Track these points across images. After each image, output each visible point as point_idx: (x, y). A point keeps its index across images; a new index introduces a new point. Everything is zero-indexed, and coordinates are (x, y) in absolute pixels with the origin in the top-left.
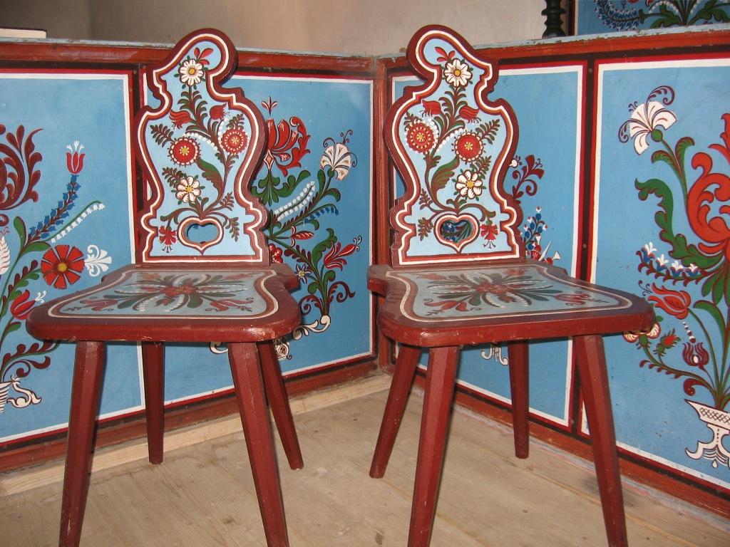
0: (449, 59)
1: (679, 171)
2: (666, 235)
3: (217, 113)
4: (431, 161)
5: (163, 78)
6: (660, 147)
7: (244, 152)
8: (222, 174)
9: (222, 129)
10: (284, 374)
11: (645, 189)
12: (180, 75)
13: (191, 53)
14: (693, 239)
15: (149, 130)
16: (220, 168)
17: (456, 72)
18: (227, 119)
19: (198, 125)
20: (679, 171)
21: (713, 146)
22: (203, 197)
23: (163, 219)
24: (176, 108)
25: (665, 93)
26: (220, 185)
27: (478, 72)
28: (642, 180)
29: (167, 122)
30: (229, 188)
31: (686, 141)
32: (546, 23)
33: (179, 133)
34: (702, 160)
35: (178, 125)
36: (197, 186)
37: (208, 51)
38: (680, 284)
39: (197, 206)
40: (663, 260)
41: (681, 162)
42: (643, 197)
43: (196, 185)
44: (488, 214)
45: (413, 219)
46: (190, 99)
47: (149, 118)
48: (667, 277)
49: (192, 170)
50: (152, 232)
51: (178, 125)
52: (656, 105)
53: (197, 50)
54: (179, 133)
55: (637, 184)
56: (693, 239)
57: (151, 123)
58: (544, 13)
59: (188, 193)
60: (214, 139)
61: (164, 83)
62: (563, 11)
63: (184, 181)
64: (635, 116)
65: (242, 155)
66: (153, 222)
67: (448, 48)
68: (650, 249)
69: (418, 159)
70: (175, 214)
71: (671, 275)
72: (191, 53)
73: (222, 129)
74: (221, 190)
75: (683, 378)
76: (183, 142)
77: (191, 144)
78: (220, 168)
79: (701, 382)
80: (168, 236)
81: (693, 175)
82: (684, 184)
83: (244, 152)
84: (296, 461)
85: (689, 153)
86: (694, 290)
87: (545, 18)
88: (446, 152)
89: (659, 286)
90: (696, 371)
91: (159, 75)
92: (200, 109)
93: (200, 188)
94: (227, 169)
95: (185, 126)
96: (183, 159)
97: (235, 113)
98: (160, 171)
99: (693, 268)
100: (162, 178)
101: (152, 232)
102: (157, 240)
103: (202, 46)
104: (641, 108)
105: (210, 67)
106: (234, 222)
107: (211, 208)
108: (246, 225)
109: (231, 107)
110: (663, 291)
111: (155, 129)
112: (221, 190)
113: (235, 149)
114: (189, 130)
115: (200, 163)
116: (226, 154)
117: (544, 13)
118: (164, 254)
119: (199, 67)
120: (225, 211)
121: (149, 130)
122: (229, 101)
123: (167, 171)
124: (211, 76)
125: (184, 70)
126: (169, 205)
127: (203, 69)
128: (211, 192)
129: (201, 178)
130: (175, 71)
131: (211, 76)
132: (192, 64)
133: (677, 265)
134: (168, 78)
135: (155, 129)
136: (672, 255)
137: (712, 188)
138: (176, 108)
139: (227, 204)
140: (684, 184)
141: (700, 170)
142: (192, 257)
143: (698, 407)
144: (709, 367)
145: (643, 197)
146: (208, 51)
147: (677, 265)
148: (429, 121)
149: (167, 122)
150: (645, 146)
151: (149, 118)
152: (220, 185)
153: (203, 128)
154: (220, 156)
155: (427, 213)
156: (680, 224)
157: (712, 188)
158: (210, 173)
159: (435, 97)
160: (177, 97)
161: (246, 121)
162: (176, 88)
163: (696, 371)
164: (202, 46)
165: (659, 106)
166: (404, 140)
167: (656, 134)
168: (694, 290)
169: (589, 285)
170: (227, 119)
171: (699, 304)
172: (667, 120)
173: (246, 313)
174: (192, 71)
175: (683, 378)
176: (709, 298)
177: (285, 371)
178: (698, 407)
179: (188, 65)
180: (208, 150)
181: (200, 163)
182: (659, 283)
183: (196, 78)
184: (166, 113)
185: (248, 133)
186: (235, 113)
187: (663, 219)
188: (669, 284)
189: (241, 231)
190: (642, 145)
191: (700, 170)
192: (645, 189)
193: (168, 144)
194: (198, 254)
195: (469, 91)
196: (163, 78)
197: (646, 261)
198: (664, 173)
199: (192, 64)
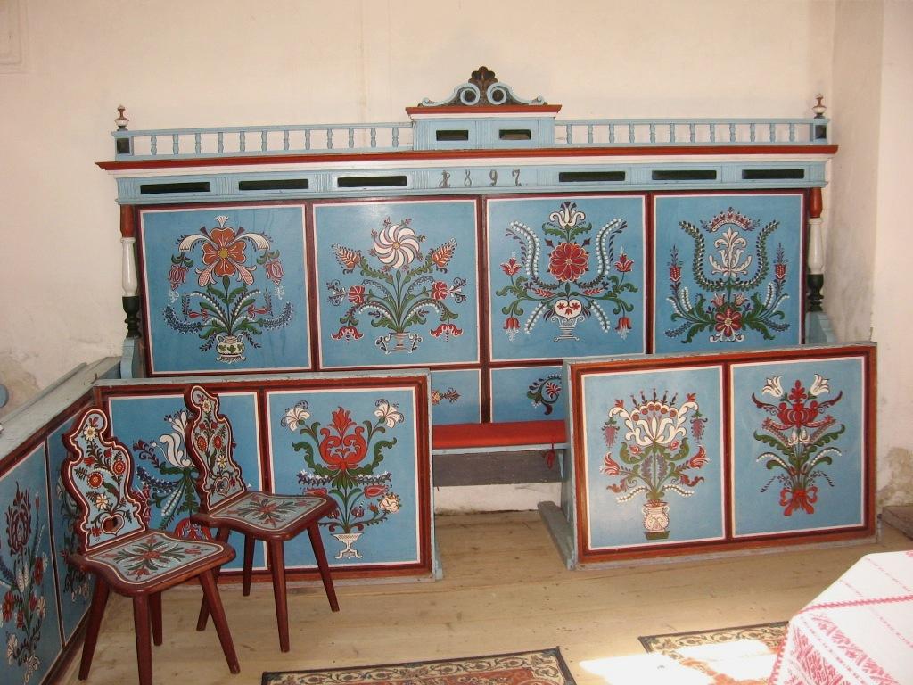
0: (202, 400)
1: (315, 437)
2: (311, 465)
3: (108, 454)
4: (208, 454)
5: (76, 439)
6: (304, 427)
7: (125, 472)
8: (117, 488)
9: (112, 462)
10: (286, 568)
11: (297, 447)
12: (84, 436)
13: (88, 422)
14: (324, 465)
15: (74, 472)
16: (115, 484)
17: (206, 406)
18: (113, 456)
19: (99, 464)
20: (315, 437)
21: (331, 425)
22: (110, 503)
23: (92, 522)
24: (86, 456)
25: (305, 404)
26: (117, 494)
27: (213, 403)
28: (296, 443)
29: (83, 465)
30: (122, 495)
31: (316, 424)
32: (128, 328)
33: (91, 470)
34: (325, 431)
35: (89, 465)
36: (106, 499)
37: (96, 419)
38: (321, 485)
39: (108, 510)
40: (311, 477)
41: (315, 434)
42: (297, 450)
43: (105, 497)
44: (231, 474)
45: (208, 487)
46: (92, 449)
47: (73, 465)
48: (314, 483)
49: (102, 489)
50: (88, 532)
51: (89, 465)
52: (299, 409)
53: (90, 419)
54: (91, 470)
55: (293, 445)
56: (324, 465)
57: (74, 468)
58: (126, 322)
59: (102, 503)
60: (109, 469)
61: (77, 443)
62: (139, 320)
63: (99, 497)
64: (289, 414)
65: (124, 474)
66: (87, 526)
67: (201, 394)
68: (304, 472)
69: (203, 454)
70: (98, 517)
71: (318, 482)
72: (88, 422)
73: (112, 462)
74: (118, 496)
75: (328, 526)
76: (94, 475)
77: (97, 475)
78: (115, 484)
79: (337, 524)
80: (97, 532)
81: (321, 438)
82: (317, 442)
83: (125, 472)
84: (158, 641)
85: (318, 429)
86: (328, 486)
87: (127, 325)
88: (211, 448)
89: (310, 488)
90: (334, 520)
91: (73, 438)
92: (99, 454)
93: (107, 499)
94: (119, 484)
95: (93, 465)
96: (95, 485)
97: (116, 452)
98: (85, 495)
99: (326, 477)
100: (87, 499)
101: (88, 532)
102: (91, 535)
103: (92, 416)
104: (292, 411)
105: (99, 428)
106: (128, 513)
107: (115, 509)
108: (134, 513)
109: (114, 449)
110: (313, 490)
111: (77, 471)
112: (118, 496)
113: (121, 472)
114: (95, 467)
115: (105, 484)
116: (117, 476)
117: (126, 322)
118: (96, 543)
119: (93, 429)
120: (122, 508)
121: (74, 472)
122: (112, 445)
123: (88, 494)
124: (101, 433)
125: (86, 433)
126: (94, 513)
127: (96, 430)
128: (114, 500)
129: (107, 493)
130: (81, 434)
131: (101, 433)
132: (89, 428)
133: (318, 477)
134: (79, 439)
135: (77, 471)
136: (316, 473)
137: (331, 442)
138: (86, 456)
139: (123, 504)
140: (317, 442)
141: (325, 436)
142: (110, 540)
143: (337, 536)
144: (340, 517)
145: (297, 450)
146: (96, 419)
147: (318, 477)
148: (203, 434)
149: (83, 465)
150: (295, 427)
151: (73, 465)
152: (117, 494)
153: (102, 464)
154: (114, 478)
155: (212, 481)
156: (317, 459)
157: (331, 442)
158: (111, 489)
159: (202, 421)
160: (85, 449)
161: (123, 455)
162: (83, 444)
163: (334, 520)
164: (92, 416)
165: (301, 409)
166: (197, 446)
167: (300, 422)
168: (328, 486)
169: (271, 495)
170: (113, 456)
171: (331, 492)
172: (306, 416)
173: (198, 556)
174: (90, 433)
175: (328, 526)
176: (336, 488)
177: (289, 565)
178: (337, 536)
179: (87, 429)
180: (107, 476)
181: (105, 484)
182: (310, 486)
183: (93, 436)
184: (81, 460)
185: (125, 461)
186: (116, 452)
187: (309, 459)
188: (315, 486)
189: (132, 517)
190: (294, 427)
191: (325, 436)
192: (297, 447)
193: (86, 478)
194: (114, 536)
195: (212, 415)
196: (76, 439)
197: (302, 478)
198: (307, 438)
199: (89, 428)
